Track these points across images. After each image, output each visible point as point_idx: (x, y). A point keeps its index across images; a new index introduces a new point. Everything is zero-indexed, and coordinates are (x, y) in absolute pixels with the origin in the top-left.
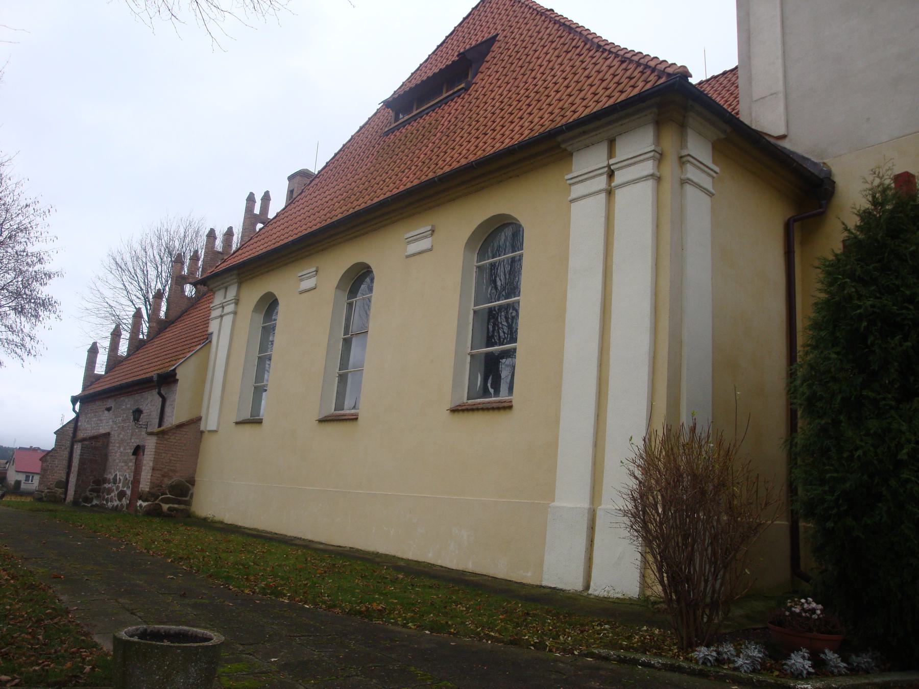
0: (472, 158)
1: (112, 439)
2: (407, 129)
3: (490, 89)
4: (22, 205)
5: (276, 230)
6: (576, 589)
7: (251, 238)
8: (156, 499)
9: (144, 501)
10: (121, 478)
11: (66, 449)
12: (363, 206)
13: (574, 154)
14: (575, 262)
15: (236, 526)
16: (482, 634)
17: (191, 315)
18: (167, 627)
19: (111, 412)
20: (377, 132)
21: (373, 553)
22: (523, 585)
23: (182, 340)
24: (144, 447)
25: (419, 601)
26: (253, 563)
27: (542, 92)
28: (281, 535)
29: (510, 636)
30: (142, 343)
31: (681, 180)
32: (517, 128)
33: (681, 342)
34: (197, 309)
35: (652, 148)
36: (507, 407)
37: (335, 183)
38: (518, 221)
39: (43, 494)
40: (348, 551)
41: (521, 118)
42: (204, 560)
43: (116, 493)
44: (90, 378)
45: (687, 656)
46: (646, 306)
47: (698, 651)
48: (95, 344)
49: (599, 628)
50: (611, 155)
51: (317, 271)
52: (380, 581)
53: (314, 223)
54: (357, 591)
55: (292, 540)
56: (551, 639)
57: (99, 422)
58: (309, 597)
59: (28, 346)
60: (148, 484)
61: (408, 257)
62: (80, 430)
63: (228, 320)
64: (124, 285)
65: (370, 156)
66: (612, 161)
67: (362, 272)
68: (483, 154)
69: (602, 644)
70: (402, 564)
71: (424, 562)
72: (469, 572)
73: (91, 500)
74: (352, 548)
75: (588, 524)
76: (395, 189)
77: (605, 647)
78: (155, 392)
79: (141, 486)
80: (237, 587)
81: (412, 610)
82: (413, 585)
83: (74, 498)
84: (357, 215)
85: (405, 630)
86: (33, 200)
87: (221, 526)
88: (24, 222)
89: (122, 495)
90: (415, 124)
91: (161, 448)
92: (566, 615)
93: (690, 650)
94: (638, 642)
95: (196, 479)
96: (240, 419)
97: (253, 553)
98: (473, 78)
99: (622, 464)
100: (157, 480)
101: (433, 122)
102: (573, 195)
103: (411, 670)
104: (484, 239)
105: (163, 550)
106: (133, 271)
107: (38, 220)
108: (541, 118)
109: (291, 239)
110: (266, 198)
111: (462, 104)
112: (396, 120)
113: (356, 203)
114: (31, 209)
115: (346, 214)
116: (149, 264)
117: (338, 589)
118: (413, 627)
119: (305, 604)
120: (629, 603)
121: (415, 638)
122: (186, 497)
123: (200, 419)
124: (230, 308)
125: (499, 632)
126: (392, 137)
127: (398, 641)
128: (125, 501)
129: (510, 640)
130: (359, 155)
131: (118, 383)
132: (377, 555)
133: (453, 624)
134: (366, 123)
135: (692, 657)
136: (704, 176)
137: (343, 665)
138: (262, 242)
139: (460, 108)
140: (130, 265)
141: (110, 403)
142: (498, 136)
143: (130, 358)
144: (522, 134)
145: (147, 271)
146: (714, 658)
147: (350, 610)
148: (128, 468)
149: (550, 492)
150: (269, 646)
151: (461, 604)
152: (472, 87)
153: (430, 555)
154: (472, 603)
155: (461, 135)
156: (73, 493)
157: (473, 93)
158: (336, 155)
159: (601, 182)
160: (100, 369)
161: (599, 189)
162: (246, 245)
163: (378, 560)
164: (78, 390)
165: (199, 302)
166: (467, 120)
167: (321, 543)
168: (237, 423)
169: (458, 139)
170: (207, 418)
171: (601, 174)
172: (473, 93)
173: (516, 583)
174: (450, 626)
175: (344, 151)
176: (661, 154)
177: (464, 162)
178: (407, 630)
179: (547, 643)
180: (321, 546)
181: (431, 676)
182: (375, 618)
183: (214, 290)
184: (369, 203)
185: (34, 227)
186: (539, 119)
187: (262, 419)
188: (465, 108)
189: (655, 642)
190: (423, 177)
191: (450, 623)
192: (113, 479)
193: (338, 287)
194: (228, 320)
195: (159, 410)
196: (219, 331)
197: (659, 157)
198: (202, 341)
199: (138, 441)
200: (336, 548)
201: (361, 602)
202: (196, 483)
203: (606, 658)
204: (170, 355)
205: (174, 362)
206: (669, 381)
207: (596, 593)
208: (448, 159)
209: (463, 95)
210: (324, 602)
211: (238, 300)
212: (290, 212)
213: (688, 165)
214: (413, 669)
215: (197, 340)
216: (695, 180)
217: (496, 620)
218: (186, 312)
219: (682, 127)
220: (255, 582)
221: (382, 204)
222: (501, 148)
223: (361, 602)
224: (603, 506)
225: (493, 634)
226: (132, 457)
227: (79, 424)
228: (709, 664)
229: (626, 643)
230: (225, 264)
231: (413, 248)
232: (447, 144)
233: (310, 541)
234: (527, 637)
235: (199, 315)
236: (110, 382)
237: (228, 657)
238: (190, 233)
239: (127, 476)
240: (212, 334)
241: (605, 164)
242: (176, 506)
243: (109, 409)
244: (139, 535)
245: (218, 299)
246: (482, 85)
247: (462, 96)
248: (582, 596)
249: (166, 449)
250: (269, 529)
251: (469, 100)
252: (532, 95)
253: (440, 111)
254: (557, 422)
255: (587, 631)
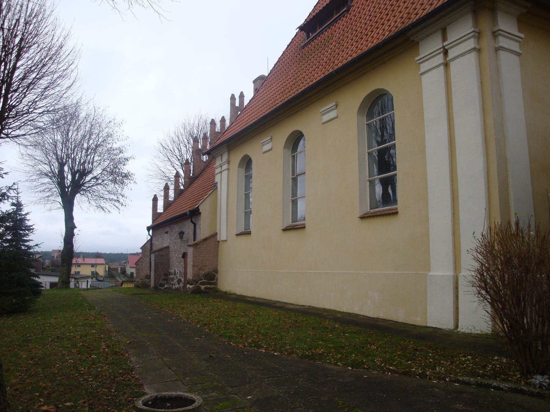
0: (355, 55)
1: (171, 249)
2: (315, 43)
3: (362, 8)
4: (107, 122)
5: (254, 110)
6: (450, 328)
7: (233, 123)
8: (196, 284)
9: (191, 285)
10: (178, 271)
11: (148, 257)
12: (293, 95)
13: (420, 43)
14: (428, 114)
15: (243, 296)
16: (385, 368)
17: (207, 172)
18: (170, 393)
19: (168, 234)
20: (297, 47)
21: (322, 309)
22: (415, 327)
23: (203, 188)
24: (187, 253)
25: (347, 344)
26: (247, 324)
27: (395, 4)
28: (269, 300)
29: (403, 369)
30: (182, 192)
31: (496, 48)
32: (381, 32)
33: (506, 159)
34: (210, 168)
35: (472, 30)
36: (395, 213)
37: (276, 83)
38: (389, 92)
39: (139, 283)
40: (307, 308)
41: (383, 24)
42: (218, 324)
43: (177, 280)
44: (156, 215)
45: (527, 382)
46: (479, 139)
47: (534, 378)
48: (155, 195)
49: (464, 359)
50: (444, 39)
51: (271, 139)
52: (324, 331)
53: (266, 109)
54: (308, 339)
55: (275, 303)
56: (430, 370)
57: (163, 240)
58: (277, 347)
59: (121, 201)
60: (192, 275)
61: (323, 123)
62: (154, 245)
63: (225, 174)
64: (169, 158)
65: (295, 63)
66: (445, 44)
67: (299, 135)
68: (356, 55)
69: (465, 373)
70: (339, 315)
71: (353, 313)
72: (381, 319)
73: (164, 285)
74: (310, 306)
75: (453, 286)
76: (311, 82)
77: (467, 375)
78: (189, 221)
79: (188, 276)
80: (235, 343)
81: (341, 352)
82: (344, 332)
83: (154, 285)
84: (290, 102)
85: (336, 367)
86: (112, 118)
87: (234, 296)
88: (109, 131)
89: (179, 281)
90: (319, 39)
91: (196, 254)
92: (442, 349)
93: (529, 377)
94: (491, 371)
95: (218, 269)
96: (239, 233)
97: (248, 316)
98: (352, 2)
99: (468, 252)
100: (196, 272)
101: (330, 35)
102: (422, 70)
103: (336, 400)
104: (369, 106)
105: (196, 319)
106: (172, 150)
107: (117, 129)
108: (396, 22)
109: (254, 121)
110: (242, 96)
111: (346, 21)
112: (308, 38)
113: (289, 94)
114: (112, 124)
115: (283, 102)
116: (181, 144)
117: (297, 339)
118: (341, 365)
119: (275, 352)
120: (486, 337)
121: (341, 373)
122: (214, 280)
123: (216, 234)
124: (225, 167)
125: (395, 366)
126: (307, 49)
127: (330, 377)
128: (181, 285)
129: (403, 372)
130: (289, 63)
131: (170, 217)
132: (325, 310)
133: (366, 362)
134: (291, 43)
135: (530, 382)
136: (512, 42)
137: (292, 399)
138: (239, 124)
139: (345, 24)
140: (170, 146)
141: (167, 229)
142: (370, 39)
143: (176, 201)
144: (384, 35)
145: (181, 149)
146: (548, 384)
147: (302, 355)
148: (181, 266)
149: (427, 266)
150: (247, 387)
151: (374, 344)
152: (351, 9)
153: (356, 309)
154: (381, 343)
155: (347, 41)
156: (153, 282)
157: (352, 13)
158: (275, 65)
159: (440, 59)
160: (160, 209)
161: (439, 64)
162: (229, 128)
163: (325, 314)
164: (150, 223)
165: (211, 163)
166: (350, 31)
167: (292, 304)
168: (237, 235)
169: (345, 44)
170: (220, 234)
171: (439, 54)
172: (352, 13)
173: (411, 325)
174: (364, 363)
175: (280, 62)
176: (479, 33)
177: (350, 59)
178: (337, 367)
179: (428, 373)
180: (292, 306)
181: (348, 404)
182: (317, 360)
183: (215, 157)
184: (297, 93)
185: (115, 133)
186: (395, 23)
187: (251, 231)
188: (348, 23)
189: (503, 370)
190: (327, 72)
191: (364, 360)
192: (174, 272)
193: (285, 147)
194: (225, 174)
195: (193, 231)
196: (221, 181)
197: (478, 35)
198: (213, 188)
199: (184, 250)
200: (301, 307)
201: (309, 349)
202: (219, 272)
203: (468, 384)
204: (196, 198)
205: (202, 198)
206: (499, 187)
207: (463, 331)
208: (340, 58)
209: (346, 15)
210: (286, 350)
211: (229, 161)
212: (252, 104)
213: (500, 37)
214: (337, 399)
215: (210, 187)
216: (506, 46)
217: (395, 356)
218: (204, 170)
219: (493, 11)
220: (246, 339)
221: (304, 93)
222: (371, 46)
223: (309, 349)
224: (462, 274)
225: (392, 368)
226: (182, 259)
227: (153, 242)
228: (544, 388)
229: (482, 372)
230: (219, 140)
231: (326, 118)
232: (339, 48)
233: (285, 303)
234: (414, 369)
235: (211, 171)
236: (165, 217)
237: (221, 397)
238: (201, 123)
239: (181, 270)
240: (217, 183)
241: (441, 46)
242: (209, 286)
243: (167, 233)
244: (184, 309)
245: (218, 162)
246: (357, 6)
247: (345, 16)
248: (454, 333)
249: (199, 254)
250: (261, 297)
251: (350, 18)
252: (389, 7)
253: (333, 28)
254: (427, 220)
255: (455, 362)
